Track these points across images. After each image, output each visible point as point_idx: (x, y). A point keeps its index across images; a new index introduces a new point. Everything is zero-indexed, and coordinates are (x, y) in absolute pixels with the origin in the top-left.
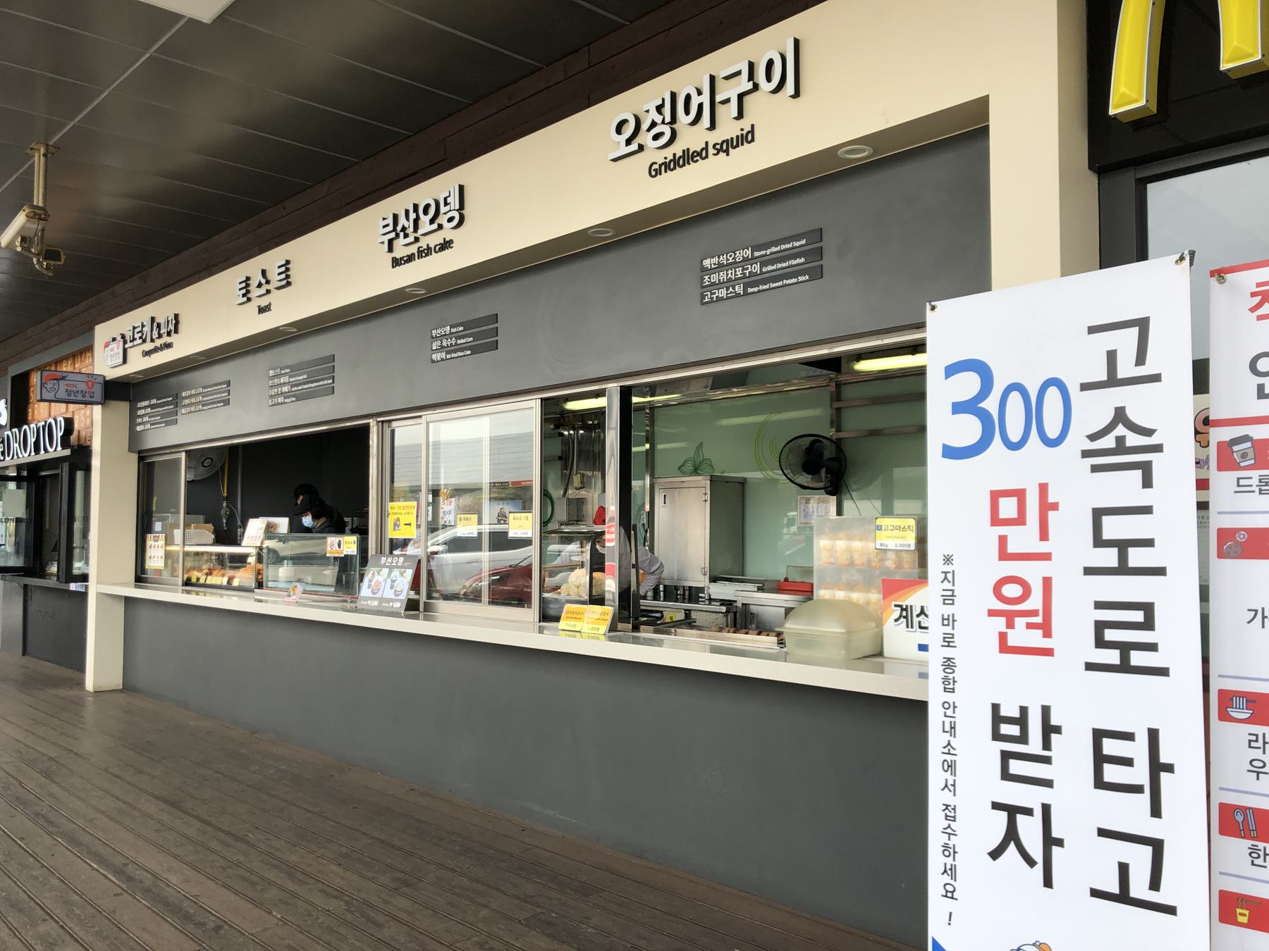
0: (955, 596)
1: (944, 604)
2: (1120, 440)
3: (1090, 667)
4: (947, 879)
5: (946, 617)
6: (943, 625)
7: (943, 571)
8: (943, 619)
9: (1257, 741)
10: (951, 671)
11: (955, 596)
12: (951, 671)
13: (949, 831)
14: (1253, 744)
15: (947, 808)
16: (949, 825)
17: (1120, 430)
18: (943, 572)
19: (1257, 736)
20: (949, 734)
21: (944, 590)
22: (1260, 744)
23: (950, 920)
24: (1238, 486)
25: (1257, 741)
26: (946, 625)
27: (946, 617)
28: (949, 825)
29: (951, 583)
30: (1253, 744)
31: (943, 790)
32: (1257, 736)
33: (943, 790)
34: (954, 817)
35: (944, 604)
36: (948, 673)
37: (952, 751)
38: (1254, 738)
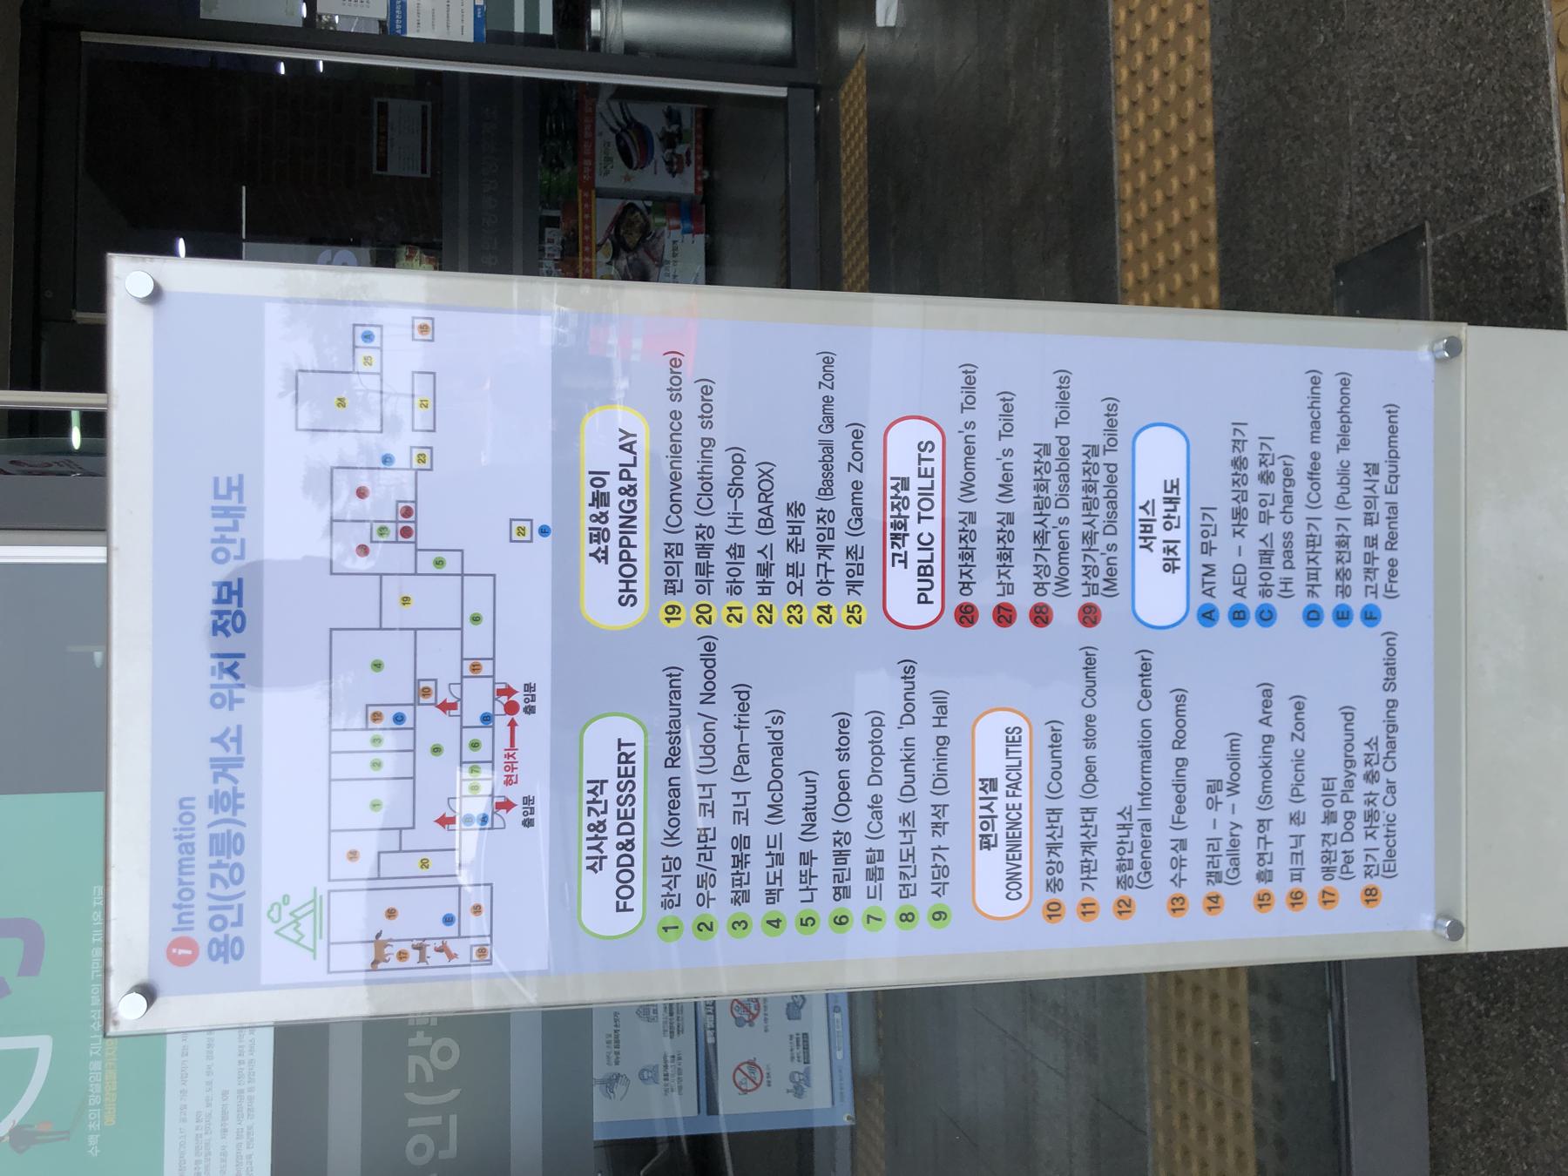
0: (231, 708)
1: (1012, 593)
2: (232, 740)
3: (634, 744)
4: (1367, 750)
5: (760, 591)
6: (769, 594)
7: (1205, 563)
8: (763, 594)
9: (705, 854)
10: (237, 945)
11: (231, 708)
12: (237, 945)
13: (1177, 880)
14: (708, 857)
15: (670, 553)
16: (1141, 508)
17: (227, 740)
18: (919, 522)
19: (700, 855)
20: (240, 520)
21: (1392, 412)
22: (707, 851)
23: (1090, 719)
24: (875, 897)
25: (705, 854)
26: (923, 602)
27: (760, 591)
28: (1141, 508)
29: (238, 660)
30: (708, 857)
31: (1152, 551)
32: (700, 855)
33: (1152, 551)
34: (678, 544)
35: (1012, 593)
36: (762, 1076)
37: (233, 734)
38: (702, 857)
